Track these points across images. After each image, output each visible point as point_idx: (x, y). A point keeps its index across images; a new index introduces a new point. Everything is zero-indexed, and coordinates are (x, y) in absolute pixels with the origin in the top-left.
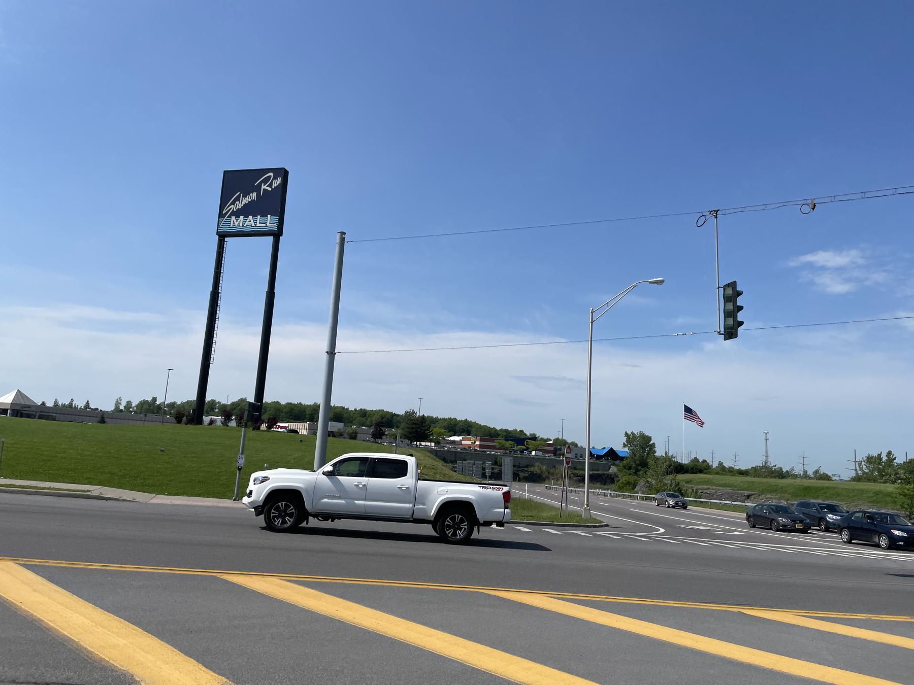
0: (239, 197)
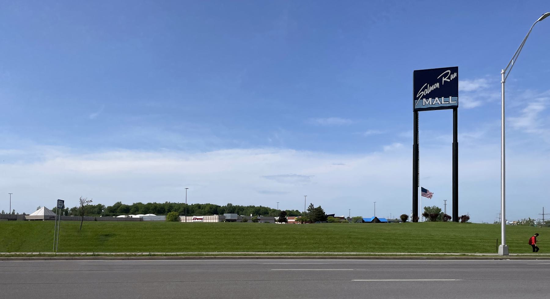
0: (427, 86)
